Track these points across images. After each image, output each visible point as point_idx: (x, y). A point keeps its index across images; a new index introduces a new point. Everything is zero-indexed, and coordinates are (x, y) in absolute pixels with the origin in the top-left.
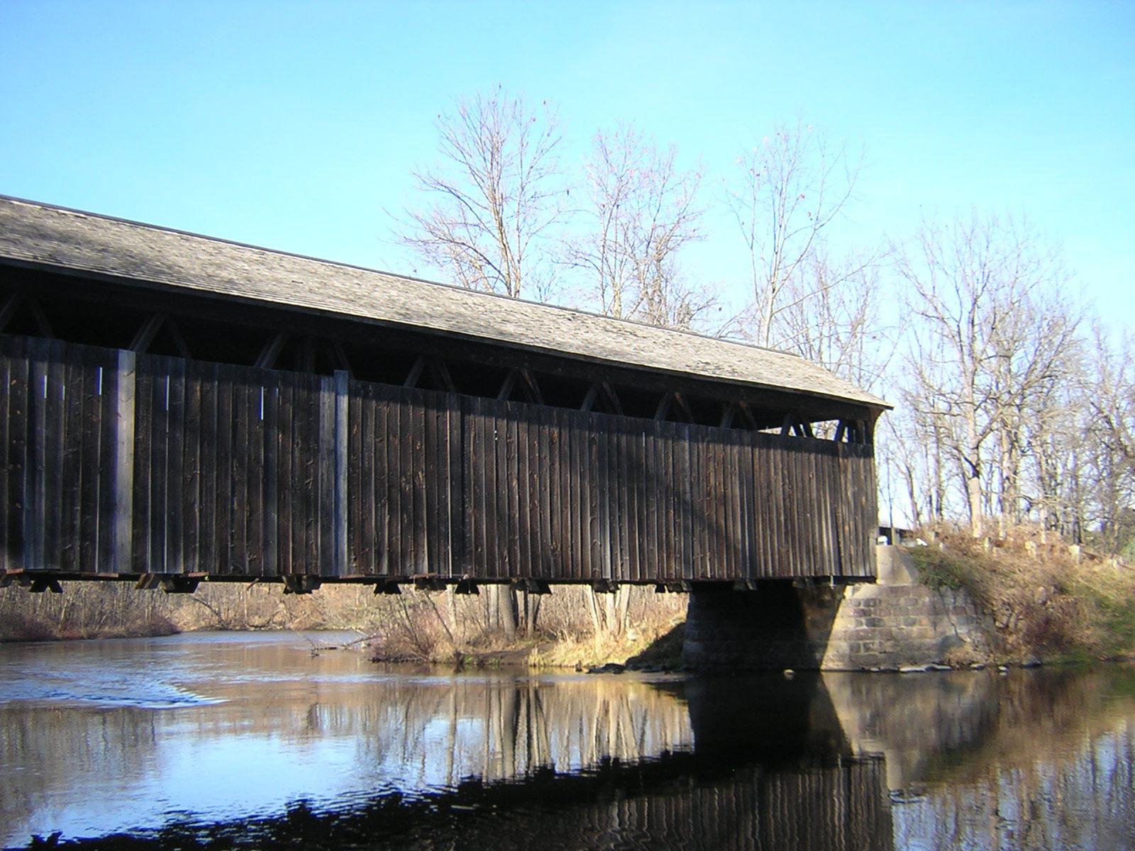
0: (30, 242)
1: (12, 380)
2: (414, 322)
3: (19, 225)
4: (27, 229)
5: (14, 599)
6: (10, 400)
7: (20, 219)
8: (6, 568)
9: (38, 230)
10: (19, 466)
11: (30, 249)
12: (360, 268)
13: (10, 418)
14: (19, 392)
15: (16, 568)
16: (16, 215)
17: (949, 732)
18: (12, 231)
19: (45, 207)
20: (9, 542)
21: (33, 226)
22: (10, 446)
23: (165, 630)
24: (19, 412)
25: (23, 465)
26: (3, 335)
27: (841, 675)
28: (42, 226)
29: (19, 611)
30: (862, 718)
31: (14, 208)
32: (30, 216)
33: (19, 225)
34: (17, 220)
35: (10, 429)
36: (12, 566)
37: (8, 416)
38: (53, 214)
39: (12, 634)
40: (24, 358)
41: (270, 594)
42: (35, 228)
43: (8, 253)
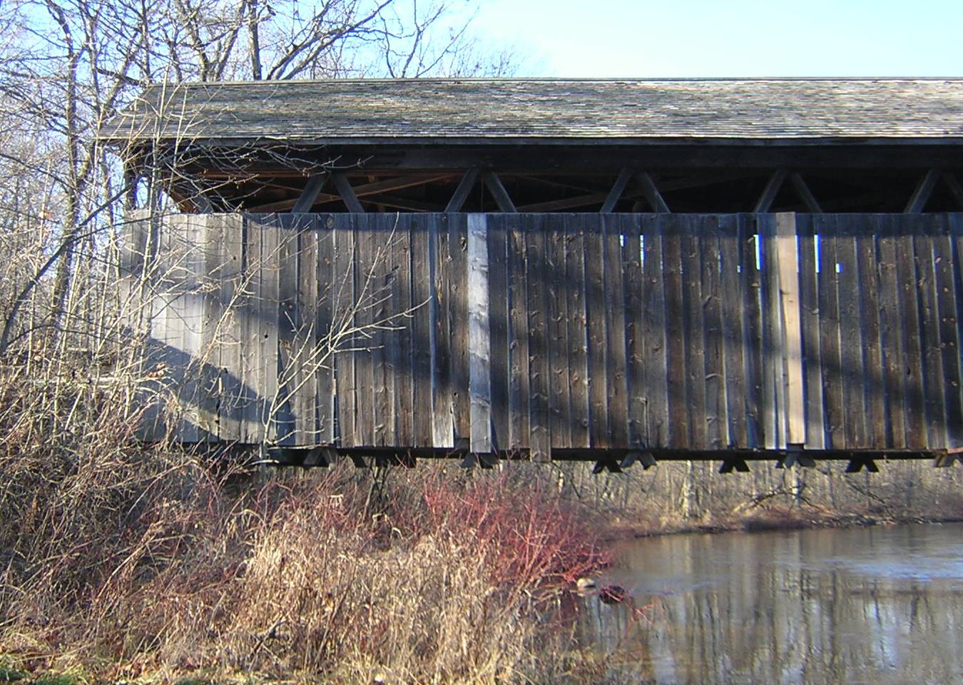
0: (939, 118)
1: (936, 259)
2: (905, 131)
3: (926, 103)
4: (935, 106)
5: (951, 479)
6: (937, 279)
7: (925, 97)
8: (947, 447)
9: (945, 105)
10: (952, 344)
11: (940, 125)
12: (724, 80)
13: (939, 297)
14: (945, 270)
15: (958, 447)
16: (921, 94)
17: (658, 440)
18: (920, 110)
19: (948, 80)
20: (948, 422)
21: (940, 102)
22: (941, 325)
23: (632, 424)
24: (946, 290)
25: (955, 342)
26: (923, 214)
27: (810, 424)
28: (949, 100)
29: (957, 491)
30: (921, 487)
31: (917, 87)
32: (934, 92)
33: (926, 103)
34: (922, 98)
35: (939, 308)
36: (953, 444)
37: (936, 294)
38: (957, 85)
39: (951, 514)
40: (946, 235)
41: (666, 388)
42: (942, 103)
43: (918, 133)
